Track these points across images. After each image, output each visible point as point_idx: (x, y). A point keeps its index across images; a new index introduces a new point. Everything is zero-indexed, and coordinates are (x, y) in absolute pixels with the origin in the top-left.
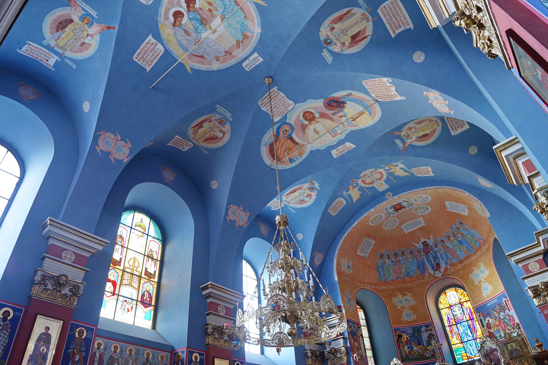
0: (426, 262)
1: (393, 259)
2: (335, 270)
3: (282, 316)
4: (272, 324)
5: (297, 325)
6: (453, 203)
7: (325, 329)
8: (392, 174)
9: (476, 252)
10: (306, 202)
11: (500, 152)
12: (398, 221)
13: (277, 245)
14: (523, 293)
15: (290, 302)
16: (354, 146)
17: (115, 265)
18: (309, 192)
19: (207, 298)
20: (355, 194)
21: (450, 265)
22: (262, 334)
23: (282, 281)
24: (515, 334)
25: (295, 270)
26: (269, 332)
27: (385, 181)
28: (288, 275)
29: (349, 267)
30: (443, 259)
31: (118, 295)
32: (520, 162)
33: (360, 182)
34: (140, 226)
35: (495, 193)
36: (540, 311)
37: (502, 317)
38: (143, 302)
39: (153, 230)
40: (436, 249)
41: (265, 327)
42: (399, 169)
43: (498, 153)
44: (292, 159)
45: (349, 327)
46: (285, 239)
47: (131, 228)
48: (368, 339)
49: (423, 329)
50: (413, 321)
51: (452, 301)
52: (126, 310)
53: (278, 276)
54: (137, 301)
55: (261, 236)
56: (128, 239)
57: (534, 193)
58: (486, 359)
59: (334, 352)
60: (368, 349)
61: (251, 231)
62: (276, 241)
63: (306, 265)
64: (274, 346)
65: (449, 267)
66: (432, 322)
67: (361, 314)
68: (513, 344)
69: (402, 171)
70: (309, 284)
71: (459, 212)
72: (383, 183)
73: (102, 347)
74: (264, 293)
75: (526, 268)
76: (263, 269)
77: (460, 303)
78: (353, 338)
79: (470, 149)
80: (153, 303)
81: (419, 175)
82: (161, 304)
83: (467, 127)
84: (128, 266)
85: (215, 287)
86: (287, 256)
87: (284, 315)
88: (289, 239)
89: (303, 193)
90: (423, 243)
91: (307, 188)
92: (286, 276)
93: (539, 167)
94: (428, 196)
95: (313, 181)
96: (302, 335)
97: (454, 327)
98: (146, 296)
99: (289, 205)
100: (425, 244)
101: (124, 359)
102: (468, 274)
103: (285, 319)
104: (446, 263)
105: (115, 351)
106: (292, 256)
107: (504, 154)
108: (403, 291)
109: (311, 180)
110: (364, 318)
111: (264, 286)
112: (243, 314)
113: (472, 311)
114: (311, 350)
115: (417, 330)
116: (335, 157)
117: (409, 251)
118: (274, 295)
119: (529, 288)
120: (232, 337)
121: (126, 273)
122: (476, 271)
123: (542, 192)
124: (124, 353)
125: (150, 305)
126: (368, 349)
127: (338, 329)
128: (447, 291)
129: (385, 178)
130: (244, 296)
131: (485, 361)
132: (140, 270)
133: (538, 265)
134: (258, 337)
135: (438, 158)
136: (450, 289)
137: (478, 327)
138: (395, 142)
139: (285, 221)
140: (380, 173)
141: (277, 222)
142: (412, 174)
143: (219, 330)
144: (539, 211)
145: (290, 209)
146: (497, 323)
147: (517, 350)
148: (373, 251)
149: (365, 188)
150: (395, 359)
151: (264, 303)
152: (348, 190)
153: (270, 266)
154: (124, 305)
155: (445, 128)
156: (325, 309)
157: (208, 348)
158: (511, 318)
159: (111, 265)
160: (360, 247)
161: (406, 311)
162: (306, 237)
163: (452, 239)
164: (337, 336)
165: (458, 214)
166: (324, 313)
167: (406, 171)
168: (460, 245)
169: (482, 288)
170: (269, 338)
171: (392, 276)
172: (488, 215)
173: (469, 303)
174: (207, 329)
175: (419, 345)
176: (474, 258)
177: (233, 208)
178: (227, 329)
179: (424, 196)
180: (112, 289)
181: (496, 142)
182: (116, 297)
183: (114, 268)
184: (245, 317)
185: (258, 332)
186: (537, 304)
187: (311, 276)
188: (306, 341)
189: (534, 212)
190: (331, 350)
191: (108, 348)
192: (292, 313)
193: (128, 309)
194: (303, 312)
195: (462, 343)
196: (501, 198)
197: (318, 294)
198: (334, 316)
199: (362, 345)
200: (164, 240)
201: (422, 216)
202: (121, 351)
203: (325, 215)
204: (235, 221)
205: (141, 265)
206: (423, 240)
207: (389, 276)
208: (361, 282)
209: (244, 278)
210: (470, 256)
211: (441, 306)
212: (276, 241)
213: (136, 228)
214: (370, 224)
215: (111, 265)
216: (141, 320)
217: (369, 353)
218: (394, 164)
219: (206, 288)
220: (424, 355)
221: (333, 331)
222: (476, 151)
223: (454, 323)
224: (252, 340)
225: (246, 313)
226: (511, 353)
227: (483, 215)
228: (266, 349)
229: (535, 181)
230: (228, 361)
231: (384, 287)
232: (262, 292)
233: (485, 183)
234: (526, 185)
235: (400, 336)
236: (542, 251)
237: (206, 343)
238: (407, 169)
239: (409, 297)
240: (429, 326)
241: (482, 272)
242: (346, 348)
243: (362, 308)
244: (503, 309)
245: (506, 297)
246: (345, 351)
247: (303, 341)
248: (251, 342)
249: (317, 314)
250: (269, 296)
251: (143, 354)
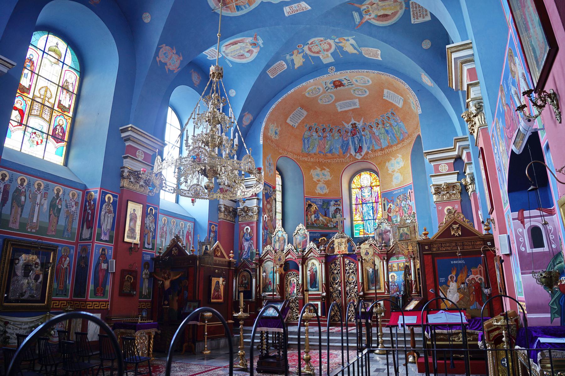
0: (350, 143)
1: (320, 134)
2: (262, 133)
3: (201, 169)
4: (191, 176)
5: (215, 181)
6: (392, 92)
7: (241, 188)
8: (341, 48)
9: (398, 144)
10: (246, 58)
11: (451, 53)
12: (334, 98)
13: (207, 97)
14: (426, 188)
15: (211, 157)
16: (310, 8)
17: (24, 93)
18: (250, 47)
19: (126, 140)
20: (298, 61)
21: (372, 151)
22: (179, 184)
23: (206, 134)
24: (409, 221)
25: (221, 125)
26: (186, 182)
27: (331, 54)
28: (214, 129)
29: (276, 133)
30: (366, 143)
31: (26, 126)
32: (466, 68)
33: (306, 48)
34: (54, 51)
35: (433, 92)
36: (435, 206)
37: (403, 205)
38: (54, 136)
39: (70, 58)
40: (363, 133)
41: (183, 177)
42: (349, 45)
43: (449, 53)
44: (240, 6)
45: (265, 189)
46: (217, 92)
47: (44, 52)
48: (281, 203)
49: (332, 203)
50: (325, 194)
51: (365, 184)
52: (35, 143)
53: (204, 129)
54: (48, 134)
55: (192, 85)
56: (39, 64)
57: (467, 101)
58: (379, 238)
59: (247, 210)
60: (279, 213)
61: (182, 78)
62: (207, 93)
63: (233, 123)
64: (189, 197)
65: (370, 152)
66: (342, 198)
67: (279, 180)
68: (405, 229)
69: (351, 47)
70: (233, 142)
71: (394, 102)
72: (330, 55)
73: (7, 179)
74: (187, 143)
75: (436, 167)
76: (189, 119)
77: (370, 187)
78: (266, 200)
79: (424, 42)
80: (66, 139)
81: (367, 56)
82: (74, 141)
83: (428, 18)
84: (39, 95)
85: (136, 131)
86: (215, 110)
87: (203, 168)
88: (221, 93)
89: (244, 48)
90: (352, 124)
91: (249, 42)
92: (212, 130)
93: (480, 77)
94: (370, 80)
95: (258, 37)
96: (219, 190)
97: (360, 206)
98: (59, 130)
99: (227, 58)
100: (354, 126)
101: (32, 193)
102: (385, 162)
103: (204, 173)
104: (368, 148)
105: (22, 184)
106: (221, 111)
107: (454, 56)
108: (322, 166)
109: (256, 35)
110: (280, 184)
111: (187, 137)
112: (162, 160)
113: (379, 195)
114: (224, 205)
115: (326, 203)
116: (286, 15)
117: (337, 129)
118: (197, 147)
119: (433, 185)
120: (147, 183)
121: (35, 103)
122: (393, 161)
123: (475, 102)
124: (31, 187)
125: (62, 140)
126: (279, 213)
127: (255, 189)
128: (362, 173)
129: (332, 50)
130: (165, 145)
131: (378, 239)
132: (52, 100)
133: (447, 168)
134: (175, 186)
135: (390, 43)
136: (366, 173)
137: (380, 210)
138: (352, 15)
139: (219, 73)
140: (329, 44)
141: (211, 73)
142: (361, 53)
143: (136, 175)
144: (466, 119)
145: (228, 62)
146: (397, 210)
147: (407, 234)
148: (303, 122)
149: (310, 56)
150: (301, 225)
151: (185, 153)
152: (292, 55)
153: (196, 117)
154: (32, 137)
155: (407, 13)
156: (245, 169)
157: (122, 191)
158: (410, 208)
159: (18, 91)
160: (291, 116)
161: (321, 185)
162: (239, 95)
163: (380, 126)
164: (252, 196)
165: (392, 104)
166: (243, 173)
167: (355, 48)
168: (386, 134)
169: (394, 177)
170: (186, 188)
171: (316, 150)
172: (420, 111)
173: (378, 188)
174: (123, 172)
175: (326, 216)
176: (394, 148)
177: (165, 48)
178: (143, 174)
179: (366, 78)
180: (19, 118)
181: (451, 42)
182: (23, 127)
183: (21, 95)
184: (163, 165)
185: (175, 181)
186: (435, 200)
187: (237, 134)
188: (221, 195)
189: (460, 119)
190: (244, 208)
191: (14, 180)
192: (212, 167)
193: (37, 142)
194: (223, 168)
195: (363, 220)
196: (436, 99)
197: (240, 153)
198: (252, 176)
199: (274, 208)
200: (83, 72)
201: (359, 98)
202: (29, 184)
203: (263, 75)
204: (166, 64)
205: (54, 96)
206: (353, 121)
207: (312, 149)
208: (285, 150)
209: (168, 126)
210: (391, 146)
211: (353, 186)
212: (207, 93)
213: (50, 53)
214: (307, 95)
215: (18, 91)
216: (52, 154)
217: (279, 216)
218: (346, 38)
219: (125, 130)
220: (327, 225)
221: (249, 191)
222: (429, 46)
223: (361, 202)
224: (169, 188)
225: (164, 161)
226: (401, 235)
227: (415, 111)
228: (181, 198)
229: (472, 89)
230: (142, 206)
231: (306, 159)
232: (184, 142)
233: (427, 80)
234: (463, 92)
235: (310, 205)
236: (455, 156)
237: (121, 185)
238: (357, 47)
239: (327, 172)
240: (338, 201)
241: (398, 163)
242: (259, 208)
243: (281, 174)
244: (405, 199)
245: (411, 189)
246: (257, 211)
247: (218, 195)
248: (167, 189)
249: (236, 172)
250: (191, 148)
251: (53, 190)
